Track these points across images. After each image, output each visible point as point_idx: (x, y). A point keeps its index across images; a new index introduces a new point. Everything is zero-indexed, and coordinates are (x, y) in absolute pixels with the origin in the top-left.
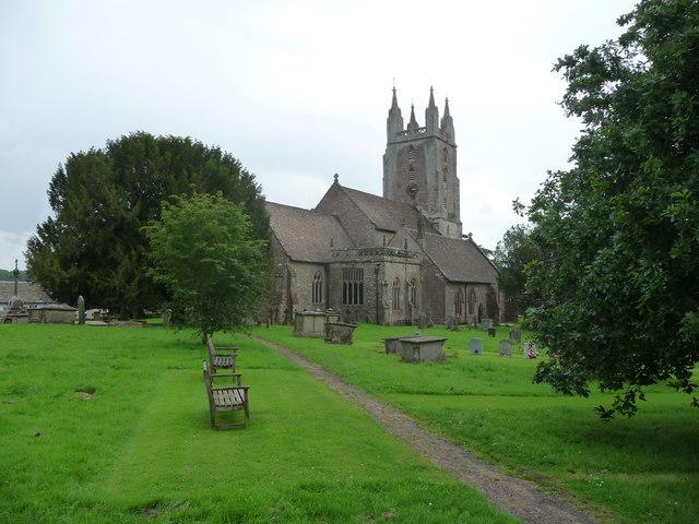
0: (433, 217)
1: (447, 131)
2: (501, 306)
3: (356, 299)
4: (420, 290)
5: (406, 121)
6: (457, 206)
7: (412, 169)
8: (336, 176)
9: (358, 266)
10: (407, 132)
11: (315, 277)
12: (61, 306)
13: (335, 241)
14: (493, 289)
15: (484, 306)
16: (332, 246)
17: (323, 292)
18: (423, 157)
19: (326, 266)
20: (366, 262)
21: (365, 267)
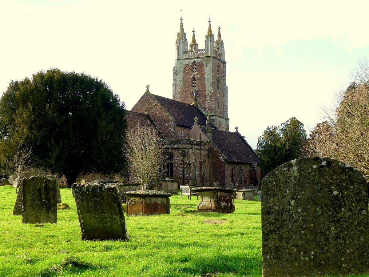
6: (225, 107)
8: (148, 86)
14: (254, 167)
20: (176, 148)
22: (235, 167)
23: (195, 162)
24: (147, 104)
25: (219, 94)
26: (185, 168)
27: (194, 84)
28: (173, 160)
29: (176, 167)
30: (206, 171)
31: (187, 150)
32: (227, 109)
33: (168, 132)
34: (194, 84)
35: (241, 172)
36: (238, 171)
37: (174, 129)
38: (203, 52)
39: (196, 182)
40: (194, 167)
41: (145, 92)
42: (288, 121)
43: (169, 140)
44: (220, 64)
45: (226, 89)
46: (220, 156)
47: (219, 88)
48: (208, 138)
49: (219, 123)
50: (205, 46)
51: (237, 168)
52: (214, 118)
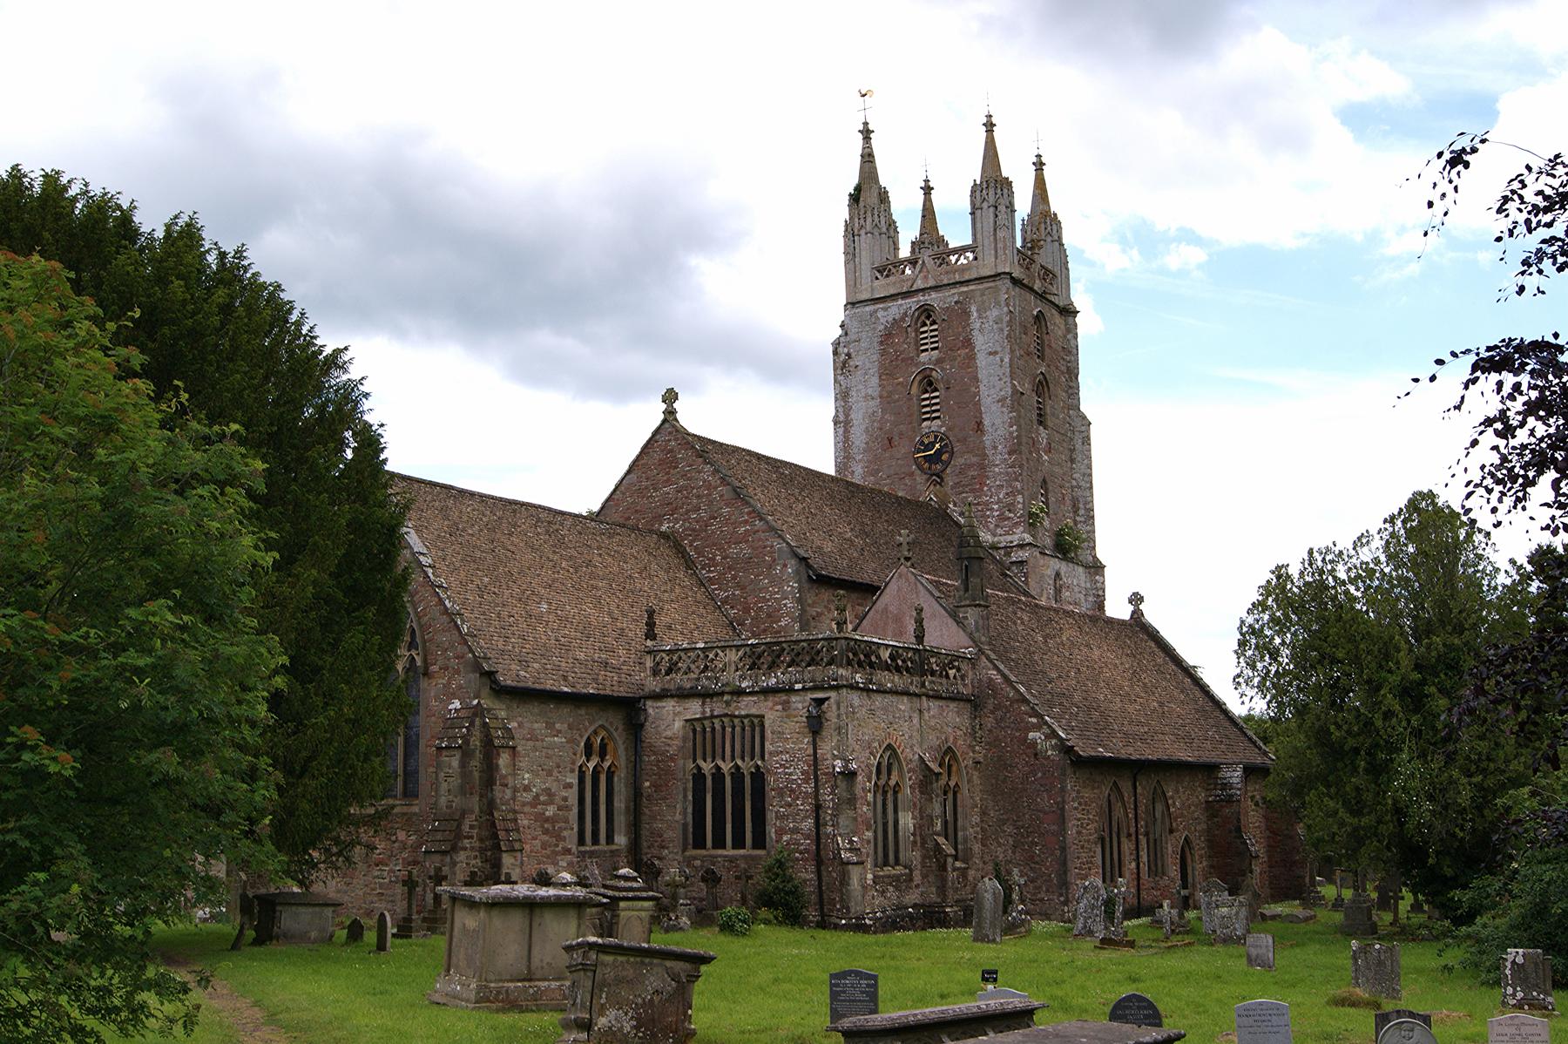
0: (1003, 540)
2: (1256, 842)
4: (972, 792)
6: (1083, 508)
7: (929, 384)
9: (747, 706)
10: (913, 262)
11: (588, 753)
12: (691, 836)
13: (661, 621)
14: (1226, 786)
15: (1200, 845)
16: (651, 635)
17: (620, 804)
18: (968, 343)
22: (1126, 787)
23: (890, 766)
24: (668, 482)
25: (1049, 450)
26: (827, 798)
27: (928, 409)
30: (959, 810)
31: (833, 694)
32: (1090, 518)
33: (769, 616)
34: (928, 409)
35: (1158, 815)
36: (1142, 809)
37: (799, 600)
39: (897, 878)
40: (885, 793)
41: (658, 423)
42: (1391, 520)
43: (738, 647)
44: (1048, 315)
45: (1083, 428)
46: (1037, 728)
47: (1050, 424)
48: (971, 636)
49: (1051, 582)
52: (1023, 555)
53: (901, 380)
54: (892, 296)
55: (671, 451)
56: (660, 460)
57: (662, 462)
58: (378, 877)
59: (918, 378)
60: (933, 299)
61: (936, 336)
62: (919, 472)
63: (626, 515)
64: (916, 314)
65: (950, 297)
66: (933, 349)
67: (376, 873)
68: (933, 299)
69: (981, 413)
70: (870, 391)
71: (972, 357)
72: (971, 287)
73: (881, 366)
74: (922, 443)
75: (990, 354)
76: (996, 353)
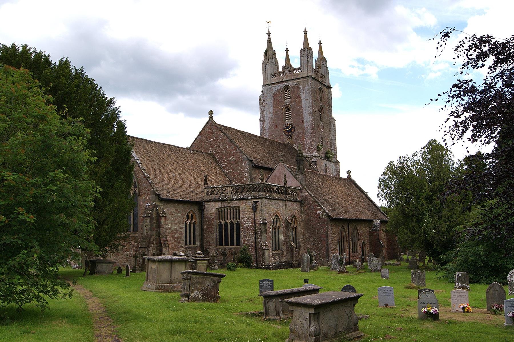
0: (310, 155)
1: (322, 71)
3: (232, 229)
4: (301, 228)
5: (281, 63)
9: (234, 204)
10: (283, 73)
11: (188, 218)
12: (147, 267)
14: (375, 226)
16: (206, 183)
17: (197, 233)
18: (299, 97)
19: (200, 205)
21: (242, 206)
24: (210, 138)
25: (323, 129)
28: (239, 219)
29: (245, 229)
30: (297, 234)
31: (260, 200)
32: (335, 148)
33: (241, 177)
35: (355, 235)
37: (250, 173)
38: (298, 72)
39: (279, 254)
40: (275, 229)
43: (232, 187)
44: (323, 88)
45: (333, 122)
46: (320, 210)
48: (300, 183)
50: (301, 64)
51: (349, 229)
52: (316, 159)
53: (279, 108)
54: (277, 83)
55: (211, 129)
56: (208, 131)
57: (209, 132)
58: (126, 255)
59: (285, 107)
60: (289, 84)
61: (290, 95)
62: (285, 135)
63: (198, 148)
64: (284, 88)
65: (294, 83)
66: (289, 99)
67: (125, 254)
68: (289, 84)
69: (303, 118)
70: (270, 111)
71: (300, 101)
72: (300, 80)
73: (274, 104)
74: (286, 126)
75: (306, 100)
76: (308, 99)
